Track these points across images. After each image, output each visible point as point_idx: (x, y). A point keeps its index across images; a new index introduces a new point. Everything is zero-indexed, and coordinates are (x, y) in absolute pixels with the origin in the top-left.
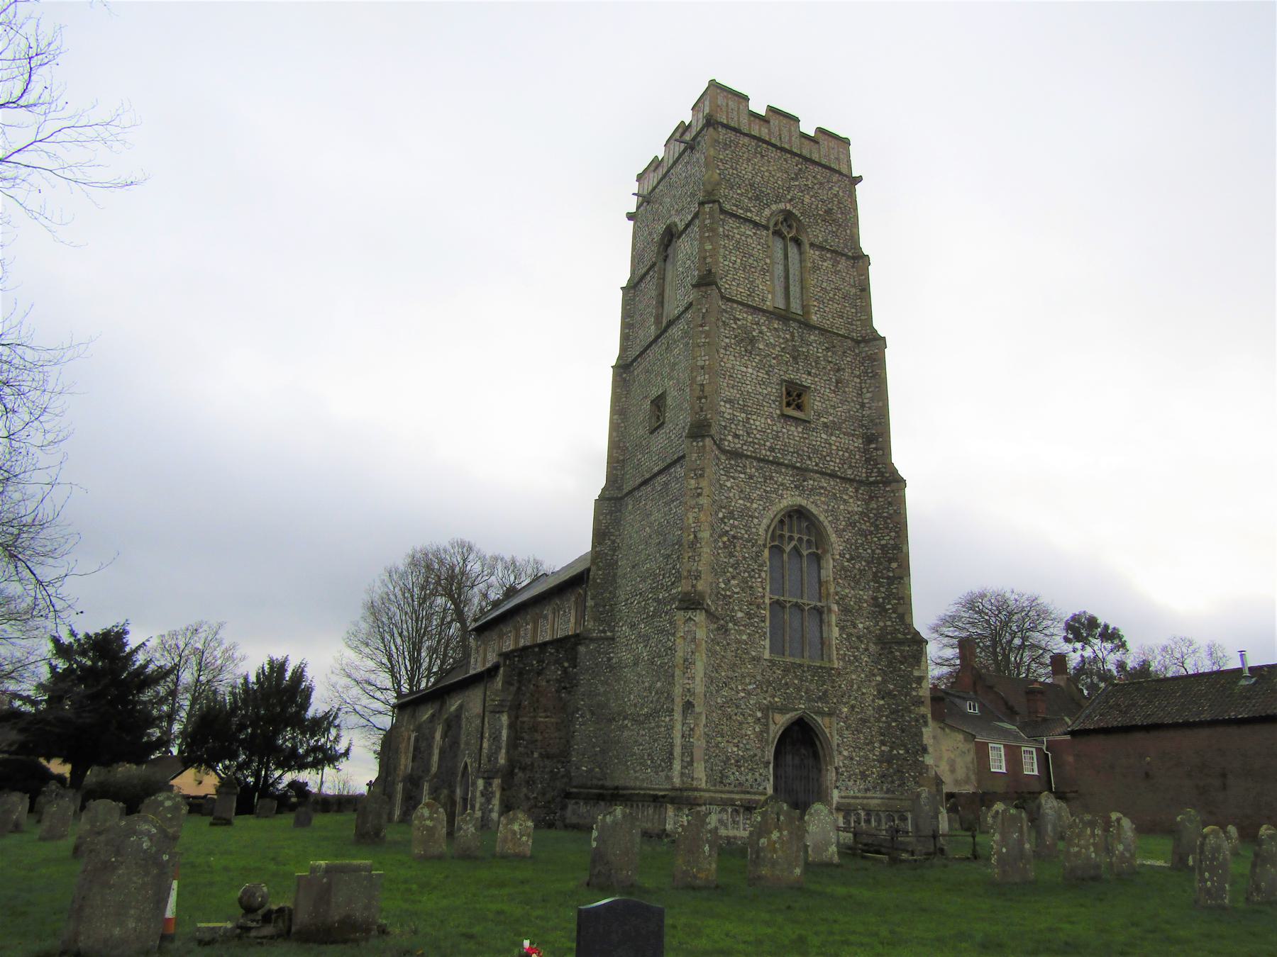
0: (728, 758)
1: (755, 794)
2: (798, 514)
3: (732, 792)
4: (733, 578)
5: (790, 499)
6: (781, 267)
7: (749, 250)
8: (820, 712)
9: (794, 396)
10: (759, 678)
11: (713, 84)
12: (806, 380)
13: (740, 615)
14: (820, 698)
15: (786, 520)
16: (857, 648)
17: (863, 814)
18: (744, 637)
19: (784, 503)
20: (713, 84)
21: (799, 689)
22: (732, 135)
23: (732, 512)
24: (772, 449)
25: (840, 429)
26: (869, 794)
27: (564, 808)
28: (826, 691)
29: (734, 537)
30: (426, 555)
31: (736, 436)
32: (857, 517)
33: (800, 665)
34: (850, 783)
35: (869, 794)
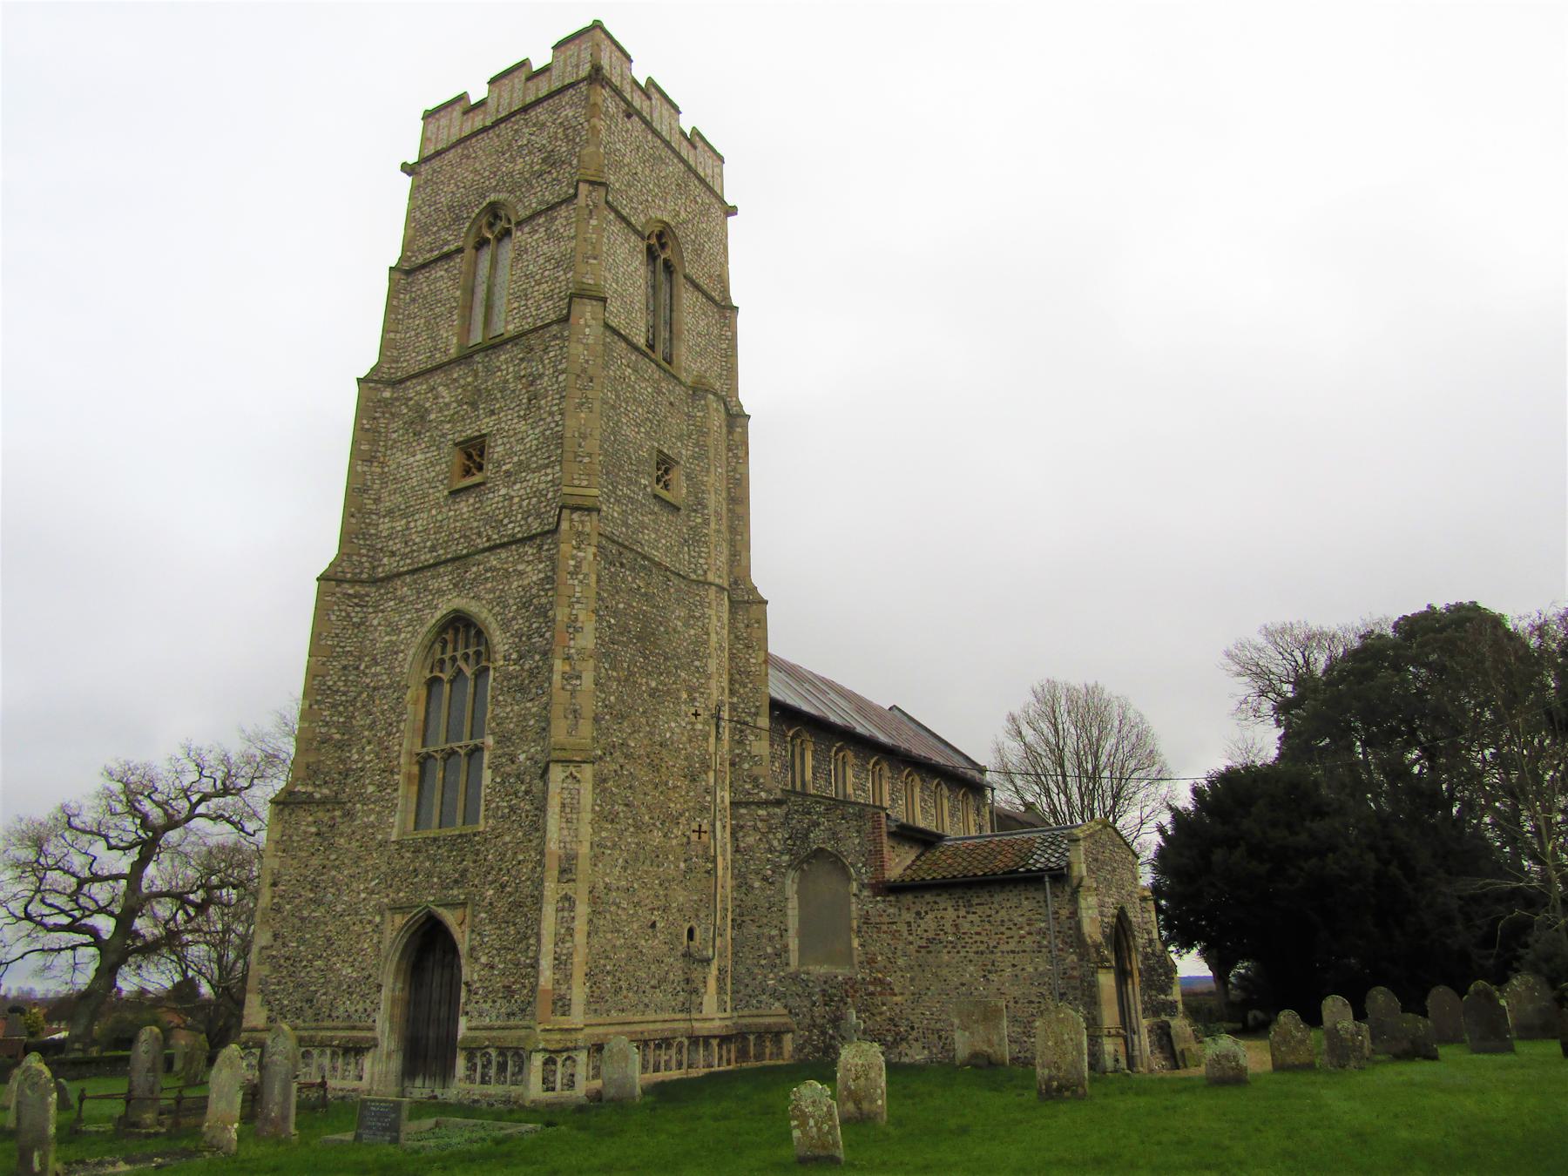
0: (340, 984)
1: (361, 1029)
2: (459, 625)
3: (491, 1028)
4: (369, 743)
5: (444, 608)
6: (485, 286)
7: (557, 256)
8: (451, 905)
9: (473, 453)
10: (383, 869)
11: (598, 25)
12: (486, 424)
13: (371, 789)
14: (456, 882)
15: (449, 636)
16: (516, 793)
17: (493, 1053)
18: (372, 818)
19: (438, 615)
20: (598, 25)
21: (429, 875)
22: (436, 163)
23: (374, 659)
24: (433, 549)
25: (528, 469)
26: (512, 1022)
27: (873, 1036)
28: (466, 870)
29: (375, 689)
30: (1055, 687)
31: (393, 554)
32: (534, 591)
33: (435, 840)
34: (487, 1006)
35: (512, 1022)
